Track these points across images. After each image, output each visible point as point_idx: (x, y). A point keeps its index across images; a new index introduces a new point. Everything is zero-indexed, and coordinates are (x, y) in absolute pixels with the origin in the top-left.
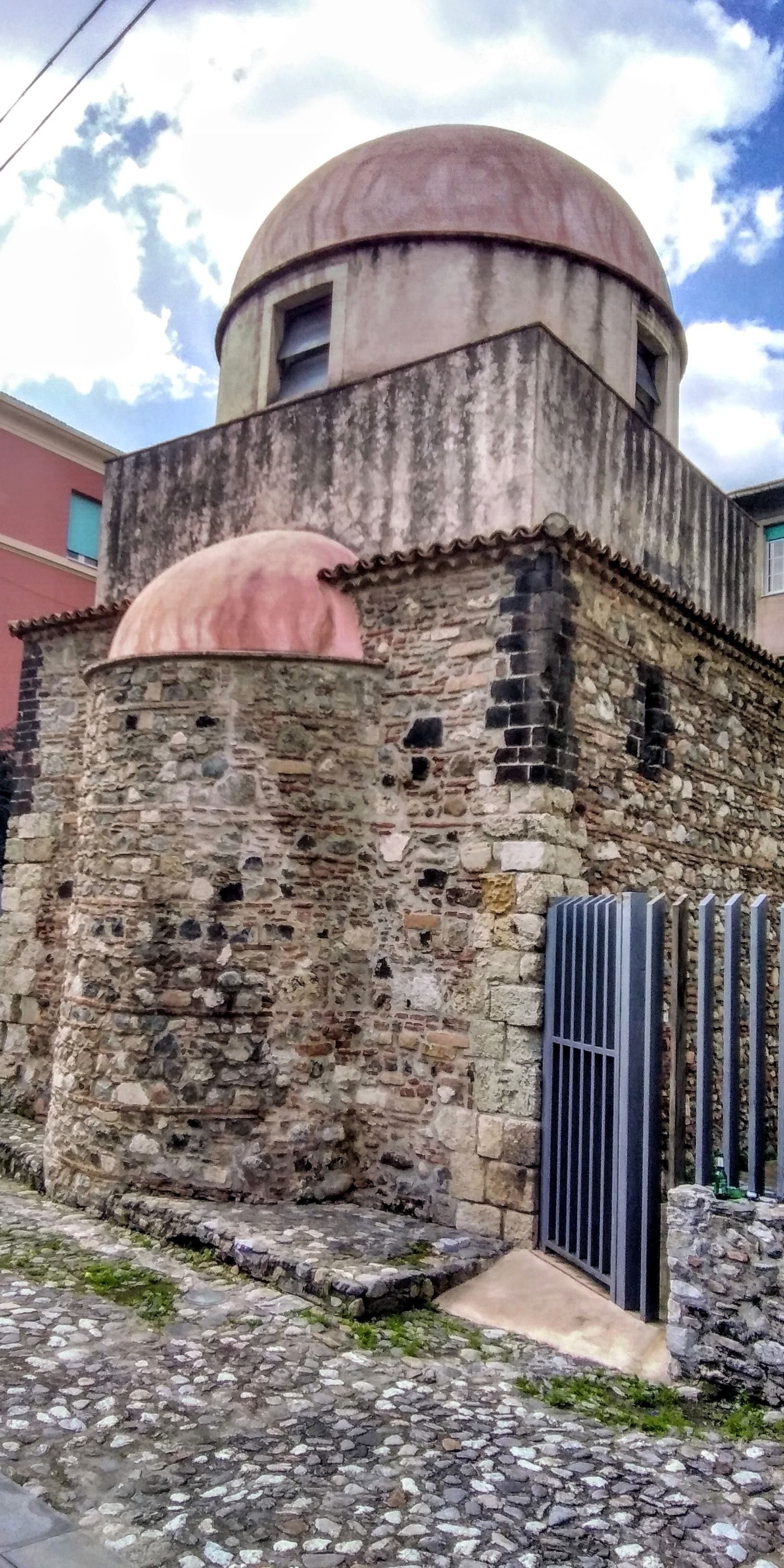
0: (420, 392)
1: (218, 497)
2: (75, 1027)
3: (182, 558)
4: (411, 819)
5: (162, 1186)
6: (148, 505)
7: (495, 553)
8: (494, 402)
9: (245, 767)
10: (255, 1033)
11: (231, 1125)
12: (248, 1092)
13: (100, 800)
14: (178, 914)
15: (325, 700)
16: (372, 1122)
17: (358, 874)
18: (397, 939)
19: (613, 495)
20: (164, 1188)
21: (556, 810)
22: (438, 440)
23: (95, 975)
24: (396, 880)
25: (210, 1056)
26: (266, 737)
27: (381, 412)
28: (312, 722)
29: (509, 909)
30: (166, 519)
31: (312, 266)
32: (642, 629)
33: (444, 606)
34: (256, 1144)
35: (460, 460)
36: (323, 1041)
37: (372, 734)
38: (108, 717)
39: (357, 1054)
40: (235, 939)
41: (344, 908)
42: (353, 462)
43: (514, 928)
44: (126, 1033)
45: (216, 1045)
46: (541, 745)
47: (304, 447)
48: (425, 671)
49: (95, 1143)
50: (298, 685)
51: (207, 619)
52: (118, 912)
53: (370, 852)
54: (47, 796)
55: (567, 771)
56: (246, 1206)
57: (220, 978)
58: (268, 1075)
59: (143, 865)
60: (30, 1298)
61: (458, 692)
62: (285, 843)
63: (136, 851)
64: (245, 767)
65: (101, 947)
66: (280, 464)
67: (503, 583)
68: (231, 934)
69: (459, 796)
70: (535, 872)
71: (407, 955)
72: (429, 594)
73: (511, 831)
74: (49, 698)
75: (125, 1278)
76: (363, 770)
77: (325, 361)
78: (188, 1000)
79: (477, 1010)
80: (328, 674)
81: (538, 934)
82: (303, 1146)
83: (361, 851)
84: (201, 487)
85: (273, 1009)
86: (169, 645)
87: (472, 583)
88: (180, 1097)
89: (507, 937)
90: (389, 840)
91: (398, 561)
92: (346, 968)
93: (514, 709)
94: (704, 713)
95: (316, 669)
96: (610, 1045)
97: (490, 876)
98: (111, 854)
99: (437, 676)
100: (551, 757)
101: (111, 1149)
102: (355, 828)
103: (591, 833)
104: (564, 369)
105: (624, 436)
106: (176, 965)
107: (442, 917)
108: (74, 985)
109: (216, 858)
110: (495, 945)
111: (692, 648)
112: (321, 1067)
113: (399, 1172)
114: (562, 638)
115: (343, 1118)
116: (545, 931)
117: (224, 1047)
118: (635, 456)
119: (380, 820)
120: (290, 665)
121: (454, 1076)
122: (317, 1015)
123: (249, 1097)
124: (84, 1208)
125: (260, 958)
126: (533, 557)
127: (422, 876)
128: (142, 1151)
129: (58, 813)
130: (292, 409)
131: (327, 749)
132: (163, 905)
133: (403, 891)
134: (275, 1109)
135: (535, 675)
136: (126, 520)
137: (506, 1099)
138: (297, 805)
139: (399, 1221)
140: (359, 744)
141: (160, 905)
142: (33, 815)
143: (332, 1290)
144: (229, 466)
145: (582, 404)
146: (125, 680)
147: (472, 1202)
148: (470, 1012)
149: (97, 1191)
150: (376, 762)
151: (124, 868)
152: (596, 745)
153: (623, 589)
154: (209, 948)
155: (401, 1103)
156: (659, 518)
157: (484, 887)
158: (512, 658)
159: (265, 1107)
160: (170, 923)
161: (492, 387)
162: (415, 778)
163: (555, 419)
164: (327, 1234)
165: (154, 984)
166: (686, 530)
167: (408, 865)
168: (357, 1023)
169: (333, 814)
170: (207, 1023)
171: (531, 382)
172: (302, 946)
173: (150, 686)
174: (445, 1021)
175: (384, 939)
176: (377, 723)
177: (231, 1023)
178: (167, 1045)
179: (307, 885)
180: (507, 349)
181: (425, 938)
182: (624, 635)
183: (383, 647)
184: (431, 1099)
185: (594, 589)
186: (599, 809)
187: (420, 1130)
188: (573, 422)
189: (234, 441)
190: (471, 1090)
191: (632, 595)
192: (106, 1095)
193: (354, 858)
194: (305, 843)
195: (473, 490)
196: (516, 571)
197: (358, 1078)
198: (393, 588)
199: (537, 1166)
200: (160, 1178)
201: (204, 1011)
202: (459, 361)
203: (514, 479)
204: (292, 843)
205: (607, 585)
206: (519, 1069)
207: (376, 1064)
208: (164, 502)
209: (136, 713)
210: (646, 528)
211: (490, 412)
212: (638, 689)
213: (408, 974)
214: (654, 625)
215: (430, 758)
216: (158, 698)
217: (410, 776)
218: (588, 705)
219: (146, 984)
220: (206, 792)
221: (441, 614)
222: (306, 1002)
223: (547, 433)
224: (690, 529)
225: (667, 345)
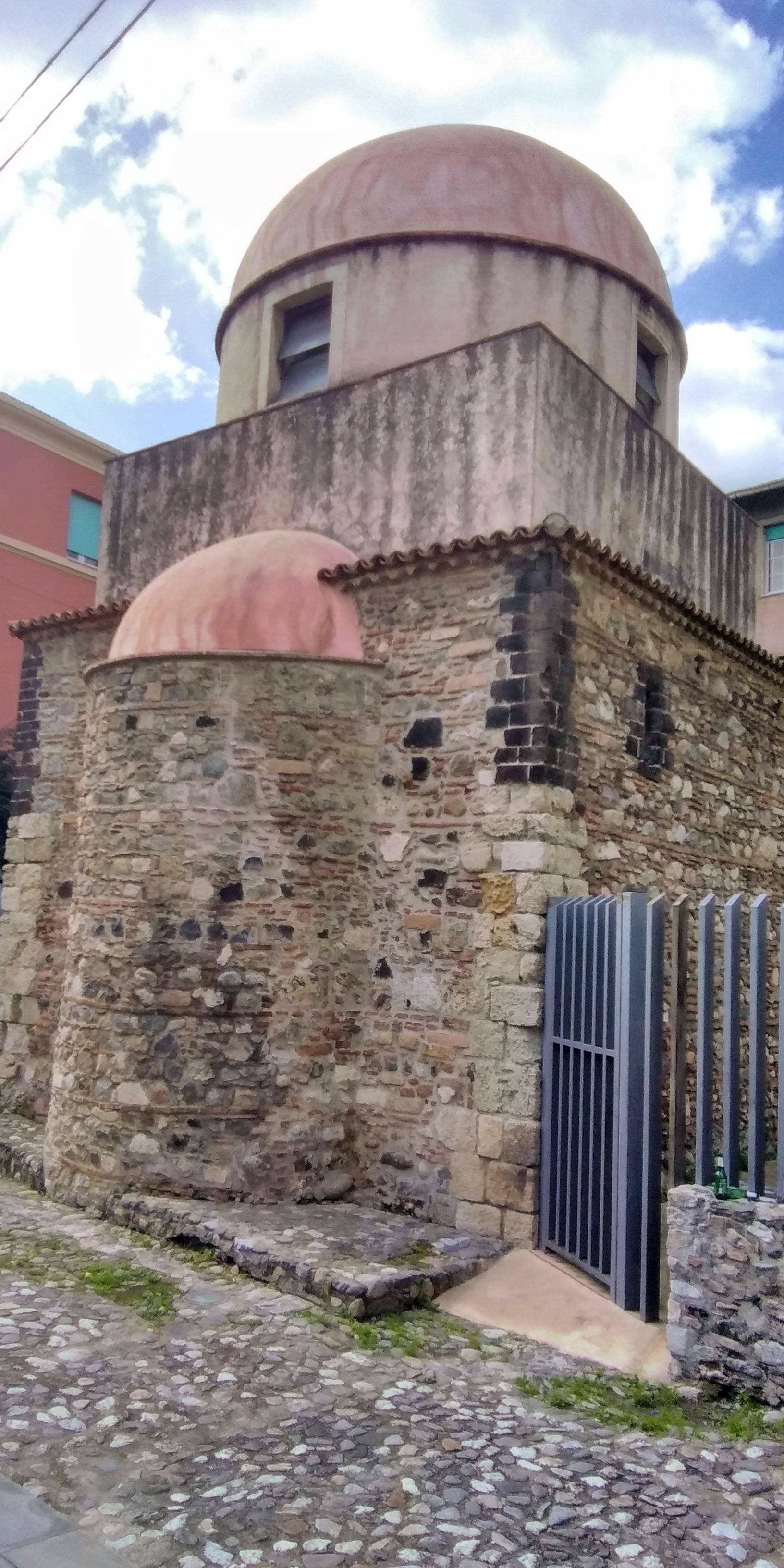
2: (75, 1027)
3: (182, 558)
4: (410, 819)
5: (162, 1186)
7: (495, 554)
9: (245, 767)
10: (255, 1033)
11: (231, 1125)
12: (248, 1092)
13: (100, 800)
14: (178, 914)
15: (325, 700)
16: (372, 1122)
17: (358, 874)
18: (397, 939)
20: (164, 1188)
21: (556, 810)
22: (438, 440)
23: (95, 975)
24: (396, 880)
25: (209, 1056)
26: (265, 737)
27: (381, 412)
28: (312, 722)
29: (509, 909)
30: (166, 519)
32: (642, 629)
33: (444, 606)
34: (256, 1144)
35: (460, 461)
36: (323, 1041)
37: (372, 734)
38: (108, 717)
39: (357, 1054)
40: (235, 939)
41: (344, 908)
42: (353, 462)
43: (514, 928)
44: (126, 1033)
45: (216, 1045)
46: (541, 745)
48: (425, 671)
49: (95, 1143)
51: (208, 619)
52: (118, 912)
53: (370, 852)
54: (47, 796)
55: (567, 771)
56: (246, 1206)
57: (220, 978)
58: (268, 1075)
59: (143, 865)
60: (30, 1298)
61: (458, 692)
62: (285, 843)
63: (135, 851)
64: (245, 767)
65: (101, 947)
66: (280, 463)
67: (503, 583)
68: (231, 934)
70: (535, 872)
71: (407, 955)
72: (429, 595)
73: (512, 831)
74: (49, 698)
75: (125, 1278)
76: (363, 770)
77: (325, 361)
78: (188, 1000)
80: (328, 674)
81: (538, 934)
83: (362, 851)
84: (201, 487)
85: (273, 1009)
86: (169, 645)
87: (472, 584)
88: (180, 1097)
89: (507, 937)
90: (389, 840)
91: (398, 560)
92: (346, 968)
93: (513, 709)
94: (704, 713)
95: (316, 669)
96: (610, 1045)
97: (490, 876)
98: (112, 854)
99: (437, 676)
100: (551, 757)
101: (111, 1149)
102: (355, 828)
103: (590, 833)
104: (564, 369)
105: (624, 436)
106: (176, 965)
107: (442, 916)
108: (75, 985)
109: (217, 858)
110: (495, 945)
111: (693, 648)
113: (399, 1172)
114: (563, 638)
115: (343, 1118)
116: (545, 931)
117: (224, 1047)
118: (635, 456)
119: (379, 821)
120: (290, 665)
121: (454, 1076)
122: (317, 1015)
123: (249, 1097)
124: (83, 1208)
125: (260, 958)
126: (533, 557)
127: (422, 876)
128: (142, 1151)
129: (58, 813)
130: (292, 409)
132: (162, 905)
133: (403, 892)
134: (275, 1109)
135: (535, 675)
136: (126, 520)
137: (505, 1099)
138: (297, 805)
139: (399, 1220)
140: (359, 744)
141: (160, 905)
142: (32, 815)
143: (332, 1290)
146: (125, 680)
147: (472, 1202)
148: (470, 1012)
149: (97, 1191)
151: (124, 868)
153: (623, 590)
154: (209, 948)
155: (401, 1103)
156: (659, 518)
157: (484, 887)
158: (512, 658)
159: (265, 1107)
161: (492, 387)
162: (415, 778)
163: (555, 419)
164: (327, 1235)
165: (154, 984)
166: (686, 530)
167: (408, 865)
168: (357, 1023)
169: (333, 814)
170: (208, 1023)
171: (531, 382)
172: (302, 946)
173: (150, 686)
174: (445, 1022)
175: (384, 939)
176: (377, 723)
177: (231, 1023)
178: (166, 1045)
179: (308, 885)
180: (507, 349)
181: (425, 938)
182: (624, 635)
183: (382, 647)
184: (430, 1099)
185: (594, 589)
186: (599, 809)
187: (420, 1130)
189: (234, 441)
190: (471, 1090)
191: (632, 595)
192: (107, 1095)
193: (354, 858)
194: (305, 843)
195: (473, 490)
196: (517, 571)
197: (358, 1078)
198: (393, 588)
199: (537, 1166)
200: (160, 1178)
201: (204, 1011)
202: (459, 361)
204: (292, 843)
205: (607, 585)
206: (518, 1069)
207: (376, 1064)
208: (164, 502)
209: (135, 713)
210: (646, 528)
211: (490, 412)
212: (638, 689)
213: (408, 974)
215: (430, 758)
217: (410, 776)
218: (588, 705)
219: (146, 984)
220: (206, 792)
221: (441, 614)
222: (306, 1002)
223: (547, 433)
224: (691, 529)
225: (667, 345)
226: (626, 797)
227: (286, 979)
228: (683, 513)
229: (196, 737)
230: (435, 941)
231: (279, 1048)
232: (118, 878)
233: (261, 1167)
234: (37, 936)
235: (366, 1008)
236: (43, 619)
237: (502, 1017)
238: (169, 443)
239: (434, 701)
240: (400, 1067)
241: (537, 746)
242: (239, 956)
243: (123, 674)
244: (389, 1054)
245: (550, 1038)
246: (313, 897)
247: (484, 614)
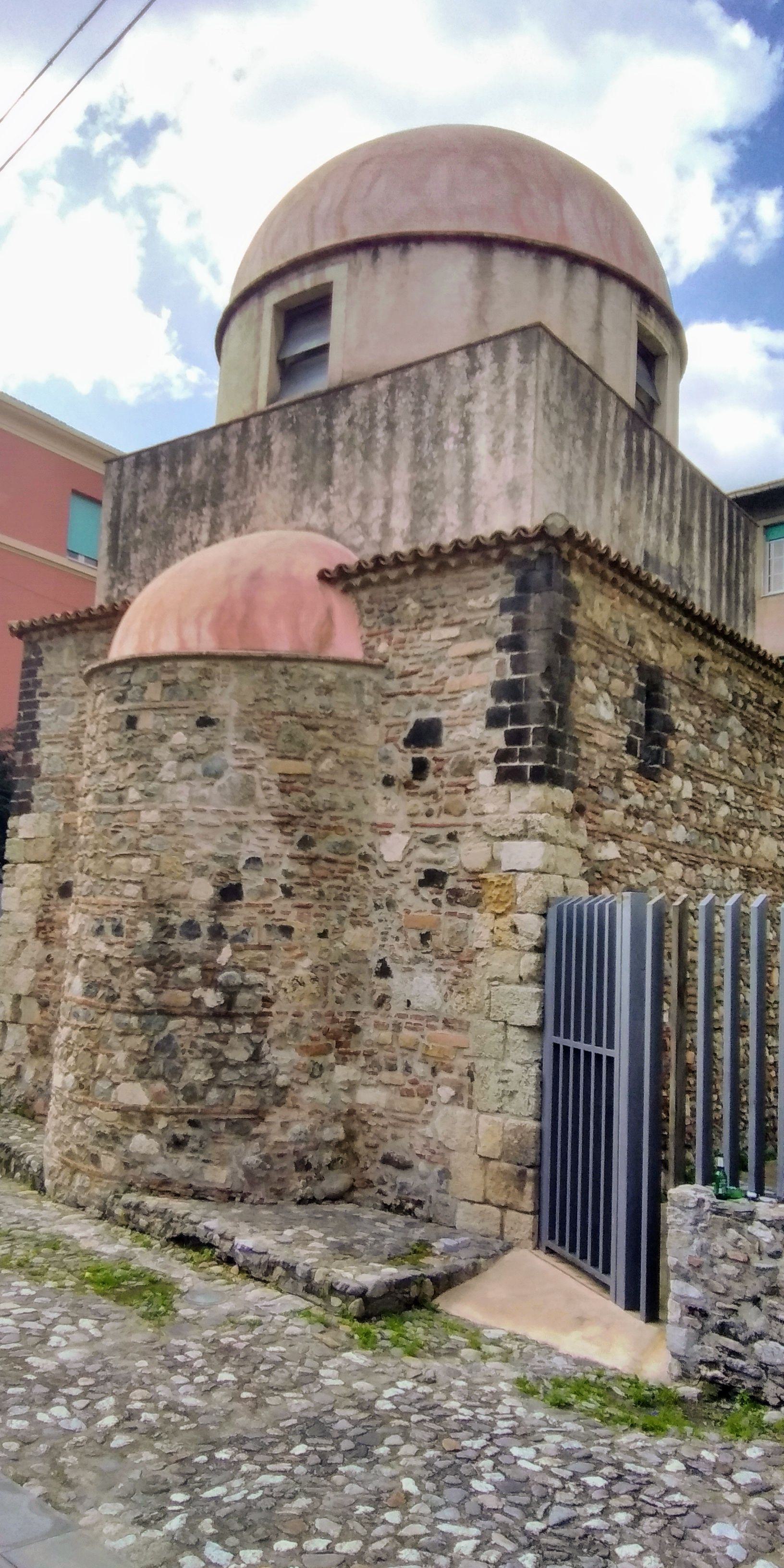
1: (218, 496)
3: (182, 558)
5: (162, 1186)
7: (495, 554)
9: (245, 767)
10: (255, 1033)
11: (232, 1125)
12: (248, 1092)
13: (100, 800)
14: (178, 914)
15: (325, 700)
16: (372, 1122)
17: (358, 874)
18: (397, 939)
20: (164, 1188)
21: (556, 810)
22: (438, 440)
23: (95, 975)
24: (396, 879)
25: (209, 1056)
26: (265, 737)
27: (381, 412)
29: (509, 909)
30: (166, 519)
31: (312, 267)
32: (642, 629)
33: (444, 606)
34: (256, 1144)
35: (460, 460)
36: (323, 1041)
37: (372, 734)
38: (108, 717)
39: (357, 1054)
40: (235, 939)
41: (344, 908)
42: (353, 461)
43: (514, 928)
44: (126, 1033)
45: (216, 1045)
46: (541, 745)
47: (304, 447)
48: (425, 671)
49: (95, 1143)
50: (297, 685)
51: (208, 618)
52: (118, 912)
53: (370, 852)
54: (47, 796)
55: (567, 771)
56: (246, 1206)
57: (221, 978)
58: (268, 1075)
59: (143, 865)
60: (30, 1298)
62: (285, 843)
63: (135, 851)
64: (245, 767)
65: (101, 947)
66: (280, 463)
67: (503, 583)
68: (231, 933)
69: (458, 796)
70: (535, 872)
71: (407, 955)
72: (429, 595)
73: (512, 831)
74: (49, 698)
75: (125, 1278)
76: (363, 770)
77: (326, 361)
78: (188, 1000)
79: (477, 1010)
81: (538, 934)
82: (303, 1146)
83: (362, 851)
84: (201, 487)
85: (273, 1009)
86: (169, 645)
87: (472, 583)
88: (180, 1097)
89: (507, 937)
90: (388, 840)
91: (398, 560)
92: (346, 968)
93: (513, 709)
94: (704, 713)
95: (316, 669)
96: (610, 1045)
97: (490, 876)
98: (112, 854)
101: (111, 1149)
102: (354, 827)
103: (591, 833)
104: (564, 369)
105: (624, 436)
106: (176, 965)
107: (442, 917)
109: (217, 858)
110: (496, 944)
111: (693, 648)
114: (563, 637)
115: (343, 1118)
116: (545, 932)
117: (223, 1047)
118: (634, 456)
119: (379, 821)
120: (289, 665)
121: (455, 1076)
122: (317, 1016)
123: (249, 1097)
124: (84, 1208)
125: (260, 958)
126: (533, 557)
127: (422, 876)
128: (142, 1151)
129: (58, 813)
130: (292, 409)
131: (327, 749)
132: (162, 905)
133: (403, 892)
134: (275, 1109)
135: (535, 675)
136: (126, 520)
137: (506, 1099)
138: (297, 805)
139: (399, 1220)
140: (359, 744)
142: (32, 815)
143: (332, 1290)
144: (229, 466)
145: (582, 404)
146: (125, 680)
147: (473, 1202)
148: (470, 1013)
149: (97, 1191)
151: (124, 868)
153: (623, 590)
154: (209, 948)
155: (401, 1103)
157: (484, 887)
158: (512, 658)
159: (265, 1107)
160: (170, 923)
161: (492, 387)
162: (415, 778)
163: (555, 418)
164: (327, 1235)
165: (154, 984)
166: (686, 530)
167: (408, 865)
168: (357, 1023)
169: (333, 814)
170: (208, 1023)
171: (531, 382)
173: (150, 686)
174: (445, 1022)
175: (384, 939)
176: (377, 723)
177: (231, 1022)
178: (166, 1046)
179: (308, 885)
181: (425, 938)
182: (624, 636)
183: (383, 648)
184: (430, 1099)
185: (594, 589)
186: (599, 809)
187: (420, 1130)
189: (234, 441)
190: (471, 1090)
191: (632, 595)
192: (107, 1095)
193: (354, 858)
194: (305, 843)
195: (473, 490)
196: (517, 571)
197: (358, 1078)
198: (393, 588)
199: (537, 1166)
200: (160, 1178)
201: (204, 1011)
202: (459, 361)
203: (514, 479)
204: (292, 843)
205: (607, 585)
207: (375, 1064)
208: (164, 502)
210: (647, 528)
211: (490, 412)
212: (638, 689)
213: (408, 974)
215: (430, 758)
216: (158, 698)
217: (410, 776)
218: (588, 705)
219: (146, 984)
220: (206, 791)
221: (441, 614)
222: (305, 1002)
224: (690, 529)
225: (667, 345)
226: (626, 797)
227: (286, 979)
228: (683, 512)
229: (196, 737)
230: (435, 941)
232: (118, 878)
234: (37, 936)
235: (366, 1008)
236: (43, 619)
237: (502, 1017)
239: (434, 701)
240: (400, 1067)
243: (124, 673)
244: (389, 1054)
245: (550, 1038)
246: (313, 897)
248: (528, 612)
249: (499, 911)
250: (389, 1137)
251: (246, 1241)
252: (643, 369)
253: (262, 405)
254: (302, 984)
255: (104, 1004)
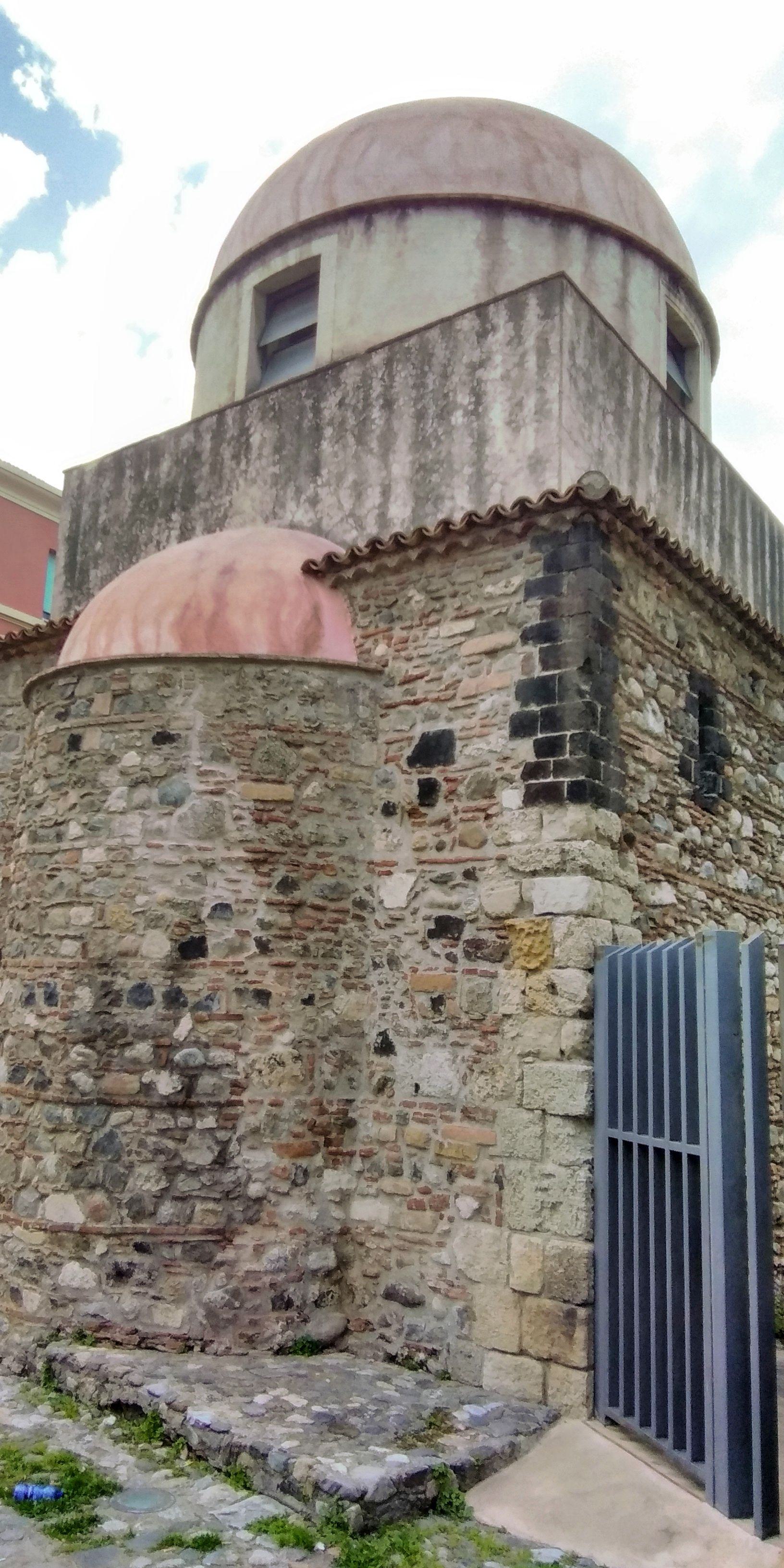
0: (423, 363)
1: (190, 496)
4: (417, 855)
5: (94, 1333)
6: (110, 515)
7: (517, 527)
8: (510, 366)
9: (212, 793)
12: (211, 1206)
13: (34, 838)
14: (126, 976)
15: (311, 711)
17: (352, 924)
18: (402, 1005)
19: (648, 484)
20: (101, 1334)
21: (601, 837)
22: (444, 415)
23: (22, 1056)
24: (399, 931)
25: (162, 1158)
26: (238, 755)
27: (377, 388)
29: (544, 963)
30: (130, 529)
32: (692, 630)
33: (454, 595)
34: (220, 1275)
35: (471, 435)
36: (309, 1138)
37: (369, 752)
39: (351, 1154)
40: (197, 1007)
41: (334, 967)
42: (345, 447)
43: (552, 988)
46: (581, 755)
47: (288, 437)
48: (432, 675)
49: (16, 1273)
50: (277, 692)
51: (171, 616)
52: (52, 975)
53: (367, 896)
55: (614, 790)
56: (208, 1359)
57: (178, 1057)
58: (238, 1184)
59: (83, 915)
61: (474, 696)
62: (261, 885)
64: (212, 793)
65: (31, 1021)
66: (260, 456)
67: (529, 562)
68: (192, 1000)
70: (578, 915)
71: (414, 1025)
73: (545, 863)
76: (357, 796)
77: (313, 345)
78: (136, 1086)
80: (315, 680)
81: (584, 994)
83: (357, 895)
84: (170, 490)
85: (245, 1097)
86: (123, 648)
87: (489, 566)
88: (125, 1212)
89: (542, 999)
90: (389, 881)
91: (399, 543)
92: (338, 1043)
93: (545, 714)
94: (761, 738)
95: (299, 673)
96: (694, 1138)
97: (519, 922)
99: (447, 679)
100: (594, 773)
101: (35, 1281)
102: (348, 867)
103: (642, 870)
104: (591, 330)
105: (658, 420)
106: (121, 1041)
107: (458, 975)
109: (175, 905)
110: (529, 1009)
111: (747, 661)
112: (306, 1173)
113: (408, 1311)
114: (604, 629)
115: (334, 1239)
116: (592, 991)
117: (182, 1146)
118: (670, 444)
119: (377, 858)
121: (478, 1182)
122: (302, 1105)
123: (214, 1212)
125: (228, 1031)
126: (565, 529)
128: (75, 1284)
130: (274, 395)
132: (106, 965)
133: (409, 944)
134: (249, 1228)
135: (571, 669)
136: (85, 534)
137: (546, 1213)
138: (276, 838)
139: (407, 1378)
140: (353, 764)
141: (103, 965)
144: (203, 464)
145: (611, 373)
146: (69, 693)
149: (16, 1337)
150: (373, 786)
151: (61, 921)
152: (644, 762)
153: (670, 579)
155: (408, 1219)
156: (698, 519)
157: (512, 937)
158: (541, 650)
159: (234, 1225)
160: (116, 987)
161: (507, 350)
162: (422, 804)
163: (582, 385)
164: (312, 1401)
165: (94, 1066)
166: (727, 539)
167: (415, 912)
168: (351, 1115)
169: (321, 849)
170: (161, 1116)
171: (554, 340)
172: (282, 1016)
173: (98, 698)
174: (465, 1111)
175: (385, 1007)
176: (374, 739)
177: (191, 1115)
178: (107, 1145)
179: (289, 938)
180: (525, 304)
182: (672, 634)
183: (381, 649)
184: (447, 1213)
185: (637, 573)
186: (651, 842)
187: (435, 1255)
188: (603, 392)
189: (208, 437)
190: (500, 1201)
191: (679, 586)
193: (347, 904)
194: (286, 885)
195: (487, 466)
196: (544, 547)
197: (353, 1186)
198: (392, 579)
200: (96, 1322)
201: (156, 1100)
202: (467, 324)
203: (536, 450)
204: (269, 885)
205: (652, 570)
206: (563, 1172)
207: (375, 1167)
208: (128, 510)
210: (685, 529)
211: (505, 377)
212: (689, 699)
213: (416, 1050)
214: (704, 627)
215: (440, 779)
217: (416, 802)
218: (634, 712)
219: (83, 1067)
220: (163, 823)
221: (452, 605)
223: (574, 400)
224: (731, 537)
225: (699, 337)
226: (680, 830)
228: (723, 518)
230: (449, 1007)
231: (252, 1148)
232: (53, 933)
233: (228, 1305)
238: (135, 446)
239: (444, 710)
240: (407, 1171)
241: (573, 756)
242: (202, 1029)
243: (67, 685)
246: (295, 953)
247: (505, 601)
248: (559, 594)
249: (532, 966)
250: (393, 1264)
251: (203, 1413)
252: (673, 366)
253: (240, 395)
254: (282, 1064)
255: (31, 1091)
